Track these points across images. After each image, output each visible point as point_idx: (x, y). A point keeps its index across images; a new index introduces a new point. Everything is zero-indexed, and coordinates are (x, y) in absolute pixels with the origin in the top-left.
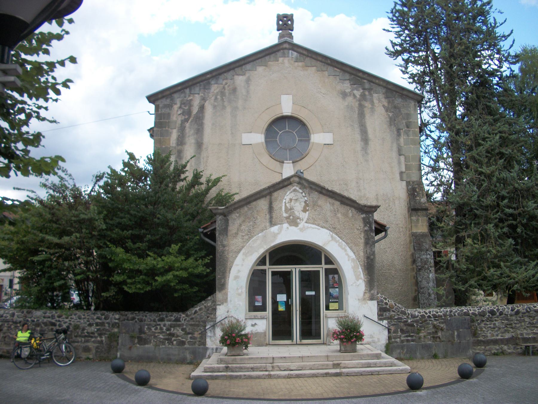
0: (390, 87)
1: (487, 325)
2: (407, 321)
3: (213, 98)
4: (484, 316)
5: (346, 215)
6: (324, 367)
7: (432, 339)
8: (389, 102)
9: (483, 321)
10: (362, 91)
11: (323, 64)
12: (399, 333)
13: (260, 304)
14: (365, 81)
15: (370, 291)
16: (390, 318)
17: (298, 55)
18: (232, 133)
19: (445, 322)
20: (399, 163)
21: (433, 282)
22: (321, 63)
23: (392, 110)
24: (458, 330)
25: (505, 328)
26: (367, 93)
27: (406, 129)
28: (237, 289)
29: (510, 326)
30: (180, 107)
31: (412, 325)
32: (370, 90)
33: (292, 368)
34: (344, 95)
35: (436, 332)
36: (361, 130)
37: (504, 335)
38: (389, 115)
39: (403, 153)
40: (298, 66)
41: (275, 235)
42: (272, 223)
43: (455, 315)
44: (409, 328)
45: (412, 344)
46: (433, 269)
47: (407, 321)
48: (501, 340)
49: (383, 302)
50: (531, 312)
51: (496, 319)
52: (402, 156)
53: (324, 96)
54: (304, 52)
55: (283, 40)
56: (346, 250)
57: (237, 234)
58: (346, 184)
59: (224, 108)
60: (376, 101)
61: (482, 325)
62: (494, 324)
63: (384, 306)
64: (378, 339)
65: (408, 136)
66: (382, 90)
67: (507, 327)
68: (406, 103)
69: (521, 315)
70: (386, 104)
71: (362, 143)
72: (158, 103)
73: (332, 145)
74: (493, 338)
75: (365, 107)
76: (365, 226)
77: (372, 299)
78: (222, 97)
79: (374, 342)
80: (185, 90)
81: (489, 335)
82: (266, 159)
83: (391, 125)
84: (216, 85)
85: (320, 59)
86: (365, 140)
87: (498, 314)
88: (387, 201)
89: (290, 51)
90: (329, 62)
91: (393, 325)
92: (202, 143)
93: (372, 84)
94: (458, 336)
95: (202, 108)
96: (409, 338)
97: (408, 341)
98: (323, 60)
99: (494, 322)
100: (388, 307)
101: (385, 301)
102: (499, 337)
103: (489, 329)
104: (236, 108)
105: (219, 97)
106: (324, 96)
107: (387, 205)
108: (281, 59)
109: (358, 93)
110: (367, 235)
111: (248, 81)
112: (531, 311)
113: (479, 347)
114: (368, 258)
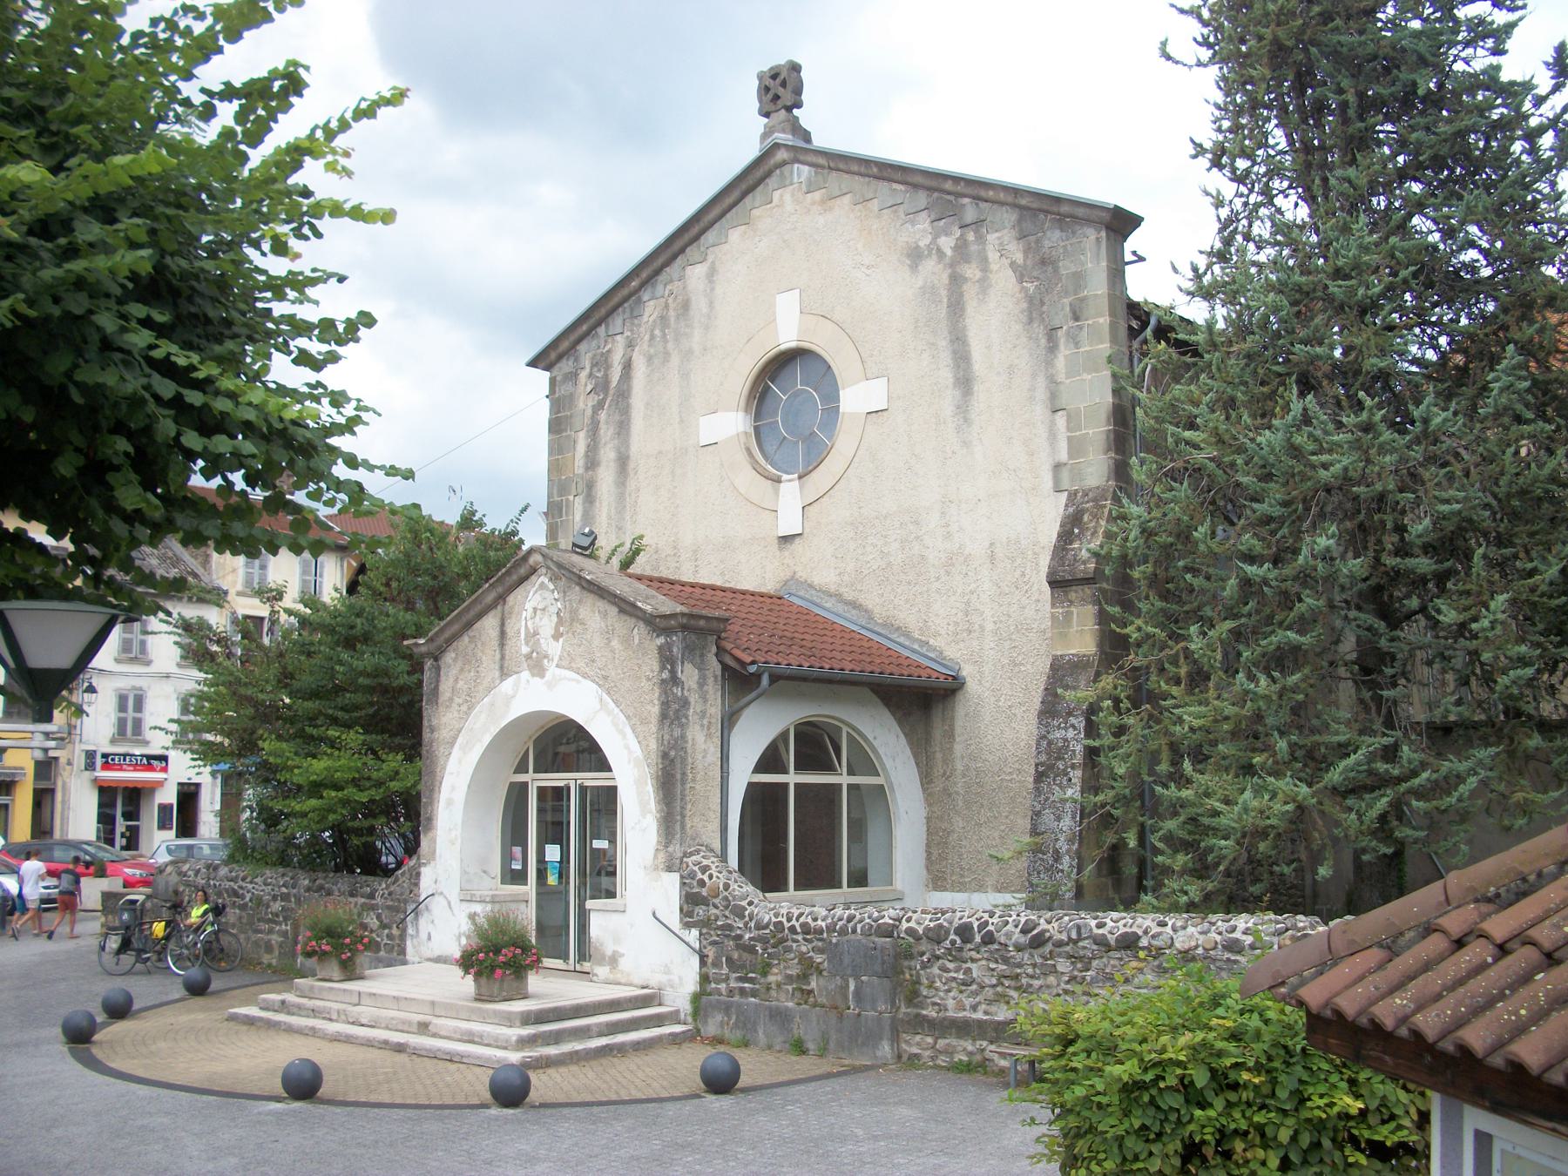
0: (1023, 202)
1: (947, 970)
2: (740, 937)
3: (647, 337)
4: (939, 943)
5: (627, 641)
6: (406, 1028)
7: (798, 994)
8: (1026, 252)
9: (938, 958)
10: (958, 233)
11: (867, 179)
12: (725, 970)
13: (519, 867)
14: (966, 200)
15: (666, 847)
16: (704, 924)
17: (813, 169)
18: (682, 421)
19: (828, 949)
20: (1052, 436)
21: (1074, 817)
22: (861, 179)
23: (1035, 274)
24: (857, 978)
25: (999, 989)
26: (971, 236)
27: (1071, 323)
28: (450, 830)
29: (1013, 983)
30: (591, 375)
31: (751, 950)
32: (978, 223)
33: (364, 1021)
34: (915, 256)
35: (804, 977)
36: (955, 352)
37: (993, 1009)
38: (1025, 290)
39: (1063, 402)
40: (813, 203)
41: (509, 699)
42: (504, 673)
43: (854, 931)
44: (746, 956)
45: (752, 1003)
46: (1077, 775)
47: (740, 937)
48: (980, 1023)
49: (693, 878)
50: (1081, 944)
51: (973, 954)
52: (1060, 413)
53: (868, 272)
54: (822, 161)
55: (769, 142)
56: (624, 736)
57: (451, 700)
58: (917, 523)
59: (667, 355)
60: (993, 255)
61: (935, 970)
62: (969, 970)
63: (695, 890)
64: (680, 978)
65: (1077, 345)
66: (1008, 217)
67: (1003, 984)
68: (1074, 240)
69: (1049, 947)
70: (1019, 257)
71: (958, 393)
72: (556, 370)
73: (885, 413)
74: (961, 1015)
75: (966, 279)
76: (663, 668)
77: (669, 869)
78: (663, 331)
79: (672, 987)
80: (598, 330)
81: (951, 1003)
82: (747, 479)
83: (1031, 321)
84: (652, 303)
85: (855, 168)
86: (965, 383)
87: (978, 939)
88: (1019, 561)
89: (796, 166)
90: (875, 170)
91: (714, 943)
92: (628, 457)
93: (983, 205)
94: (857, 992)
95: (628, 366)
96: (746, 985)
97: (742, 991)
98: (863, 170)
99: (969, 965)
100: (704, 892)
101: (700, 876)
102: (979, 1015)
103: (954, 985)
104: (688, 355)
105: (657, 332)
106: (868, 272)
107: (1017, 574)
108: (776, 195)
109: (947, 243)
110: (666, 693)
111: (712, 274)
112: (1080, 939)
113: (918, 1038)
114: (665, 755)
